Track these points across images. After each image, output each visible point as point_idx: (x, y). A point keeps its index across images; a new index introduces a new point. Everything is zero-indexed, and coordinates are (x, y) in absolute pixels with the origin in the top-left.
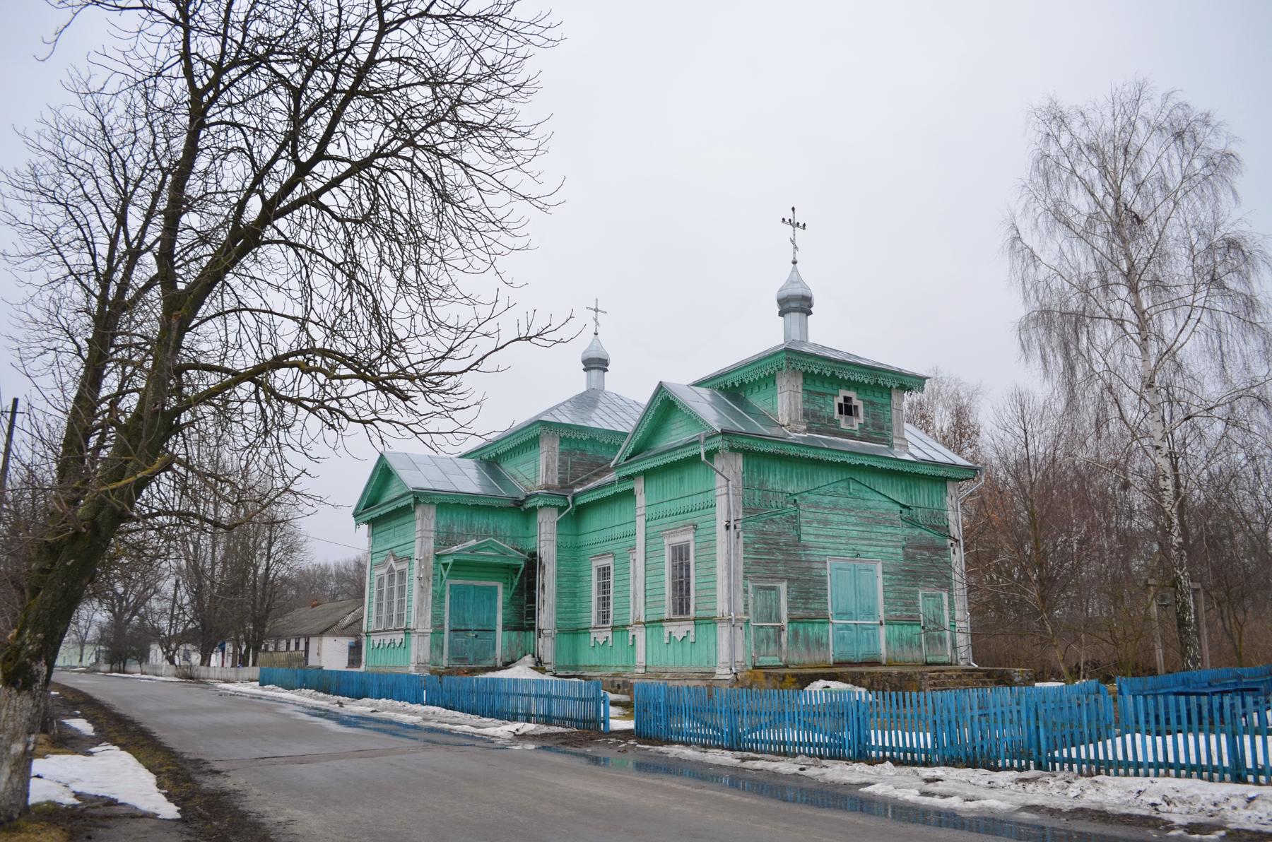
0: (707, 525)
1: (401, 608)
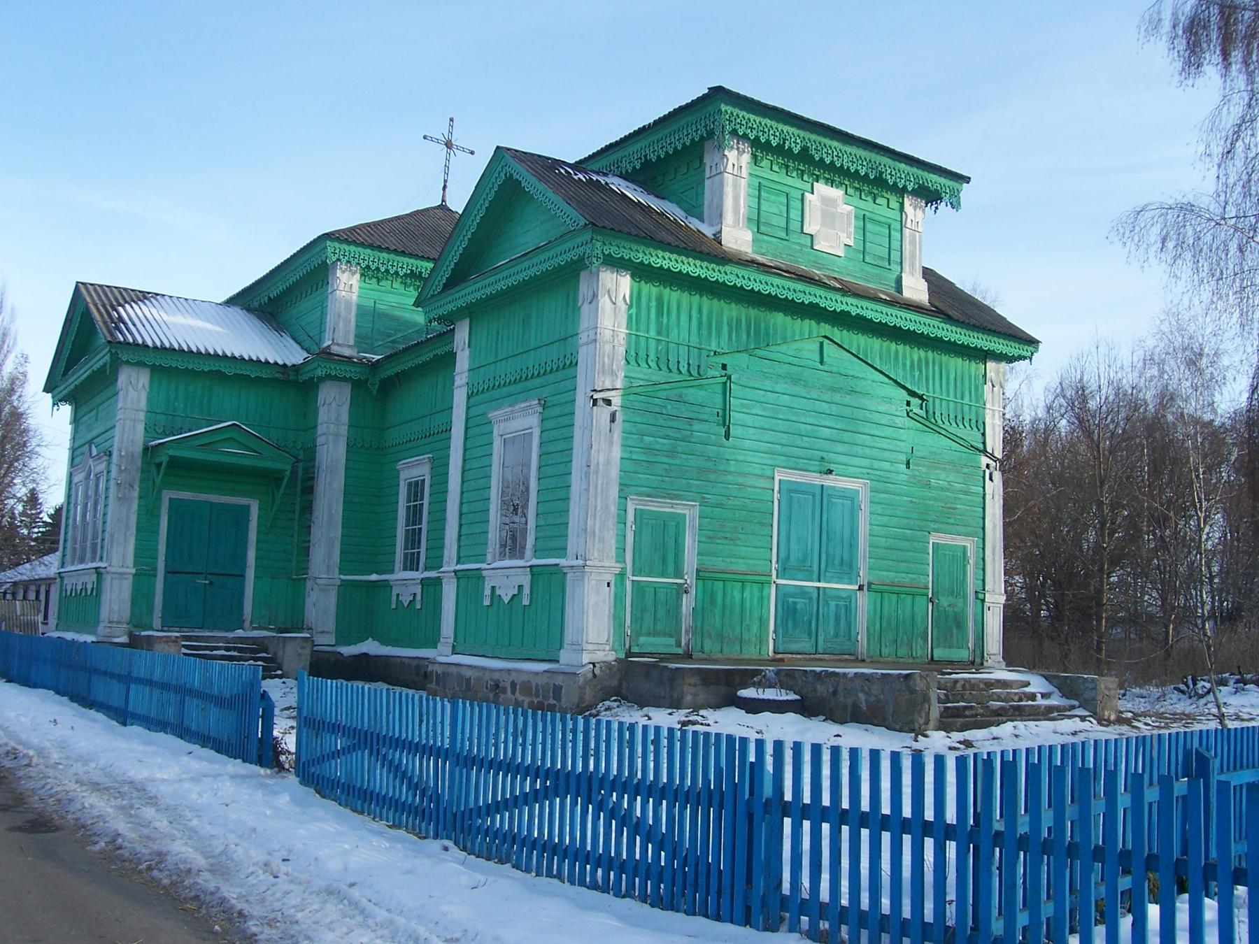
0: (562, 398)
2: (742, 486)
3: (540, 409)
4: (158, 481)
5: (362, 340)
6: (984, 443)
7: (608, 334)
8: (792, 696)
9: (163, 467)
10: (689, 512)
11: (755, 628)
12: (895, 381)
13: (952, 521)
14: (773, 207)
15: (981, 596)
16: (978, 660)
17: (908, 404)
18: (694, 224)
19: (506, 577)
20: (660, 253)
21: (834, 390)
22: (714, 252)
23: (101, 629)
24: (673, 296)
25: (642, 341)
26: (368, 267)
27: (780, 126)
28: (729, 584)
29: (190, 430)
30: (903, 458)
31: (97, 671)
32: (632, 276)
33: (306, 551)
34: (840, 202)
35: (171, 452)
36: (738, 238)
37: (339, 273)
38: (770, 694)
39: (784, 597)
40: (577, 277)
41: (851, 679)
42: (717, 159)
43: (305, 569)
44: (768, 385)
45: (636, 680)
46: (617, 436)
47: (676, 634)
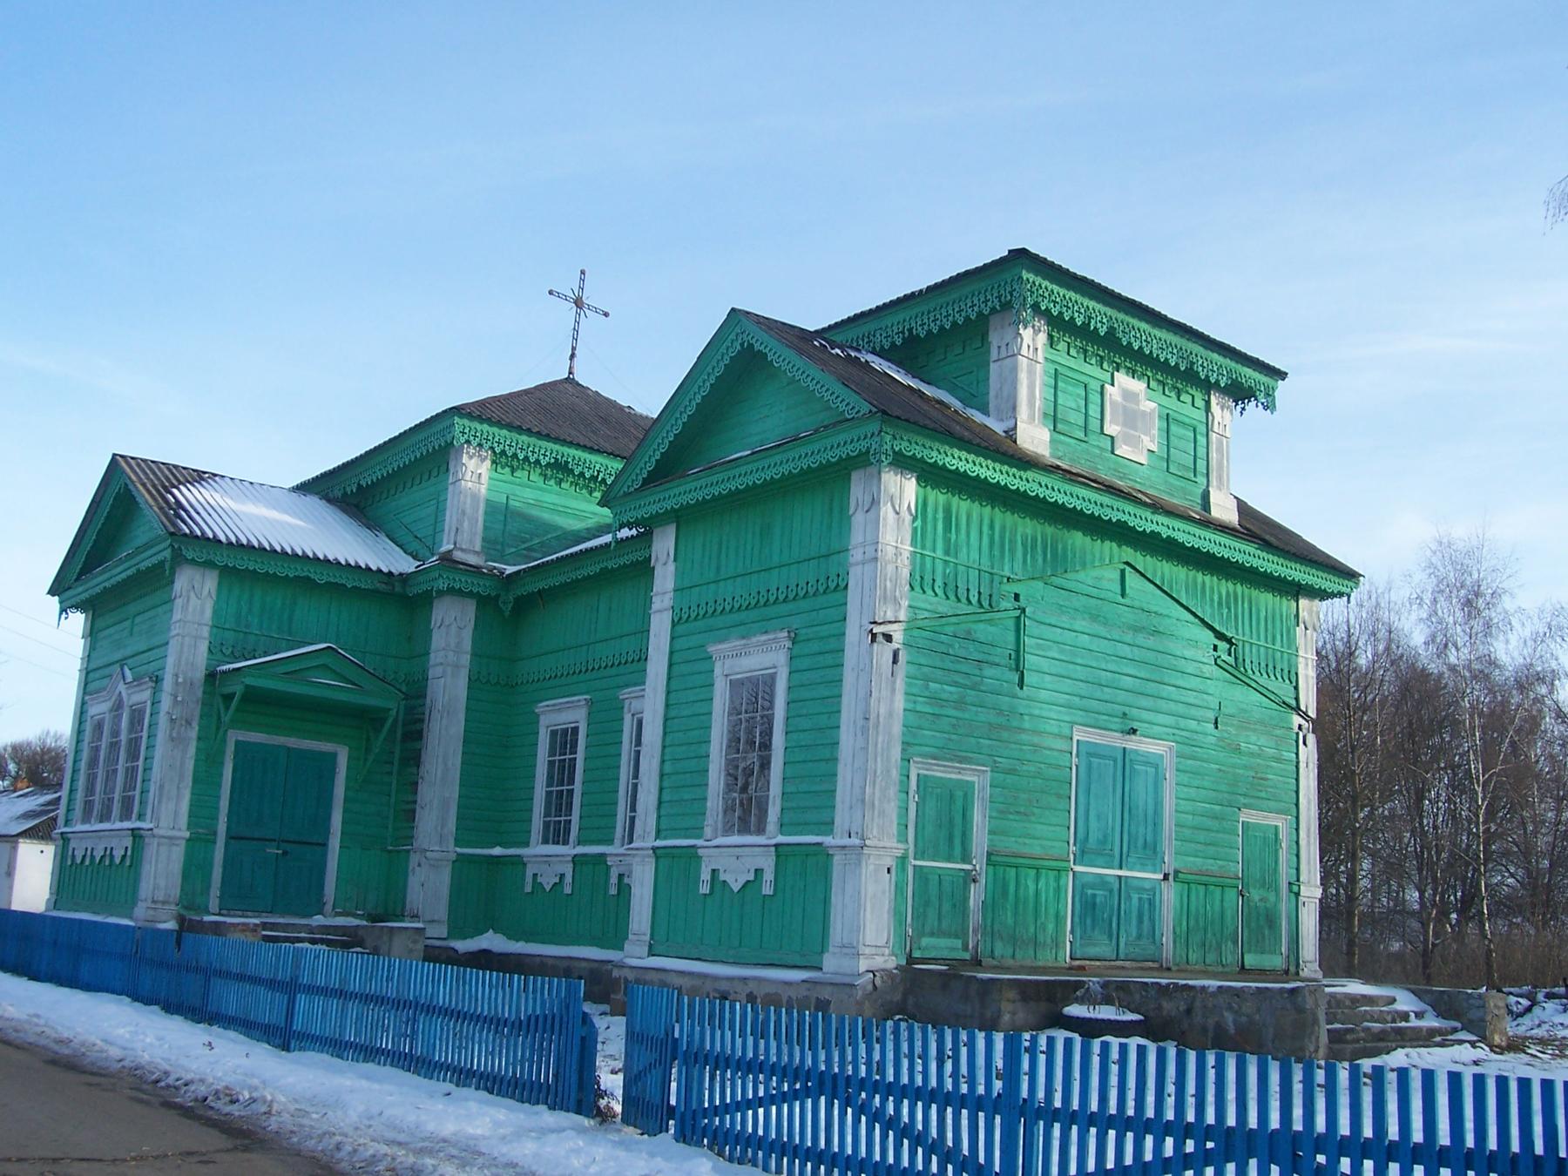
1: (130, 784)
2: (1037, 747)
3: (788, 644)
4: (226, 718)
5: (492, 546)
6: (1297, 699)
7: (890, 551)
8: (1131, 1017)
9: (226, 698)
10: (977, 778)
11: (1051, 927)
12: (1202, 620)
13: (1263, 795)
14: (1070, 400)
15: (1295, 889)
16: (1292, 969)
17: (1215, 648)
18: (978, 417)
19: (736, 858)
20: (956, 452)
21: (1137, 629)
22: (1006, 451)
23: (141, 911)
24: (963, 506)
25: (928, 561)
26: (503, 452)
27: (1086, 302)
28: (1023, 871)
29: (266, 654)
30: (1211, 715)
31: (227, 975)
32: (918, 480)
33: (411, 815)
34: (1142, 396)
35: (249, 681)
36: (1034, 437)
37: (465, 459)
38: (1107, 1013)
39: (1081, 887)
40: (847, 479)
41: (1213, 994)
42: (1008, 338)
43: (410, 838)
44: (1064, 621)
45: (932, 994)
46: (900, 684)
47: (962, 934)
